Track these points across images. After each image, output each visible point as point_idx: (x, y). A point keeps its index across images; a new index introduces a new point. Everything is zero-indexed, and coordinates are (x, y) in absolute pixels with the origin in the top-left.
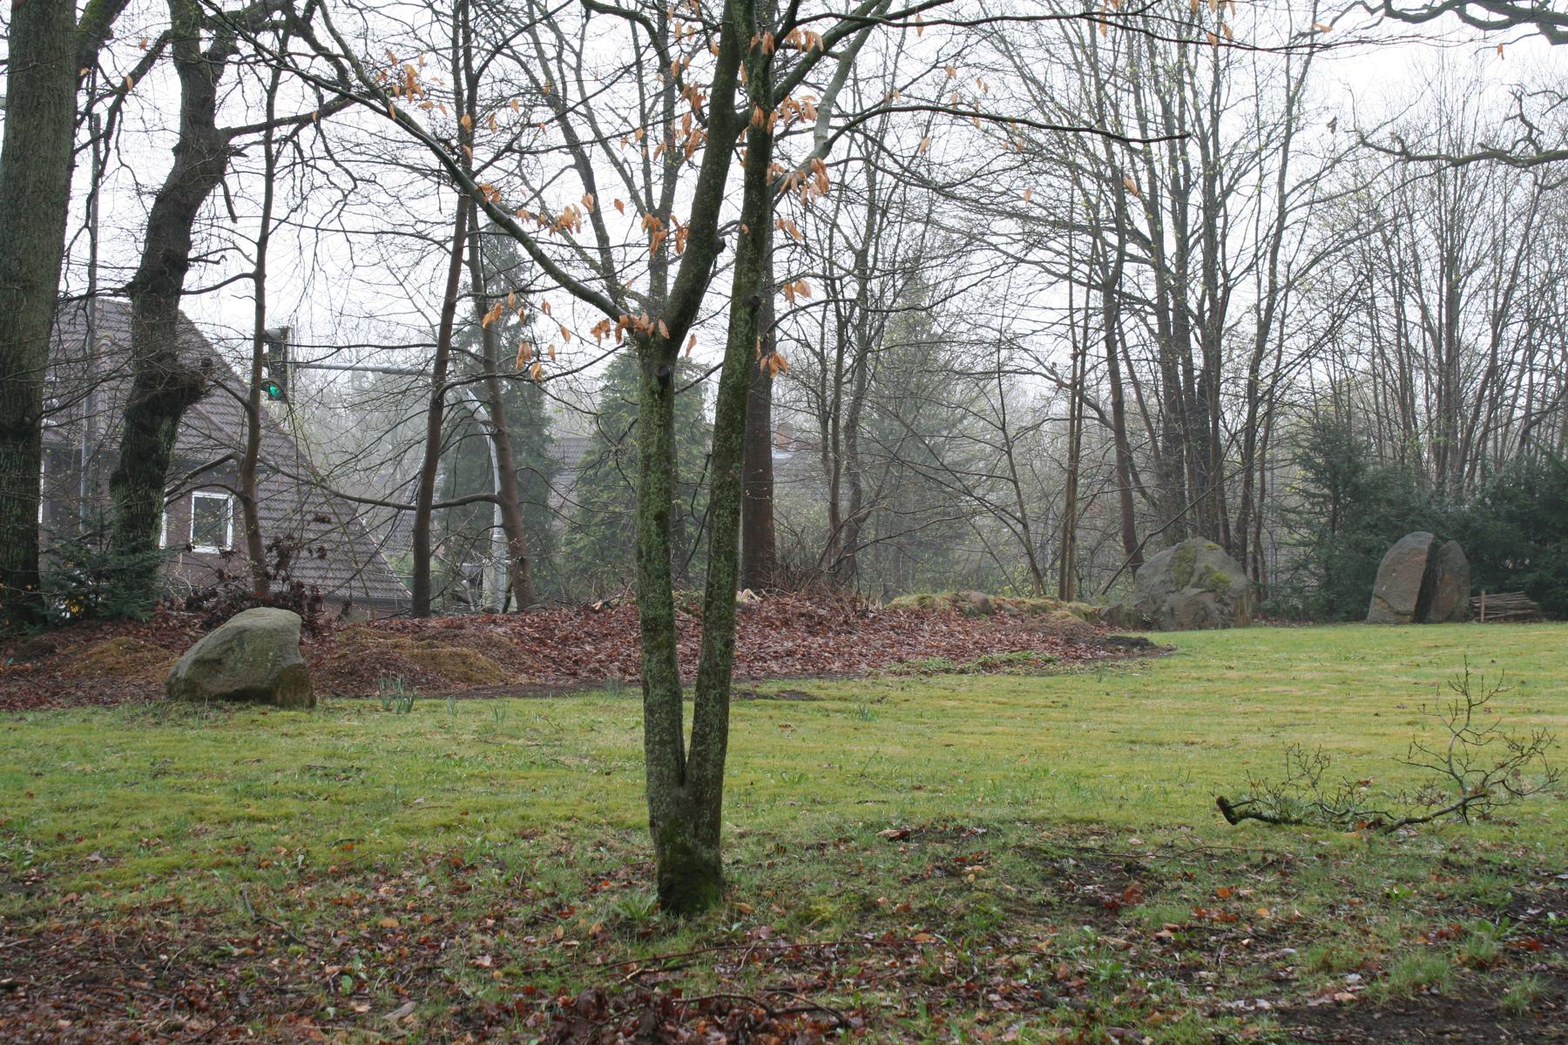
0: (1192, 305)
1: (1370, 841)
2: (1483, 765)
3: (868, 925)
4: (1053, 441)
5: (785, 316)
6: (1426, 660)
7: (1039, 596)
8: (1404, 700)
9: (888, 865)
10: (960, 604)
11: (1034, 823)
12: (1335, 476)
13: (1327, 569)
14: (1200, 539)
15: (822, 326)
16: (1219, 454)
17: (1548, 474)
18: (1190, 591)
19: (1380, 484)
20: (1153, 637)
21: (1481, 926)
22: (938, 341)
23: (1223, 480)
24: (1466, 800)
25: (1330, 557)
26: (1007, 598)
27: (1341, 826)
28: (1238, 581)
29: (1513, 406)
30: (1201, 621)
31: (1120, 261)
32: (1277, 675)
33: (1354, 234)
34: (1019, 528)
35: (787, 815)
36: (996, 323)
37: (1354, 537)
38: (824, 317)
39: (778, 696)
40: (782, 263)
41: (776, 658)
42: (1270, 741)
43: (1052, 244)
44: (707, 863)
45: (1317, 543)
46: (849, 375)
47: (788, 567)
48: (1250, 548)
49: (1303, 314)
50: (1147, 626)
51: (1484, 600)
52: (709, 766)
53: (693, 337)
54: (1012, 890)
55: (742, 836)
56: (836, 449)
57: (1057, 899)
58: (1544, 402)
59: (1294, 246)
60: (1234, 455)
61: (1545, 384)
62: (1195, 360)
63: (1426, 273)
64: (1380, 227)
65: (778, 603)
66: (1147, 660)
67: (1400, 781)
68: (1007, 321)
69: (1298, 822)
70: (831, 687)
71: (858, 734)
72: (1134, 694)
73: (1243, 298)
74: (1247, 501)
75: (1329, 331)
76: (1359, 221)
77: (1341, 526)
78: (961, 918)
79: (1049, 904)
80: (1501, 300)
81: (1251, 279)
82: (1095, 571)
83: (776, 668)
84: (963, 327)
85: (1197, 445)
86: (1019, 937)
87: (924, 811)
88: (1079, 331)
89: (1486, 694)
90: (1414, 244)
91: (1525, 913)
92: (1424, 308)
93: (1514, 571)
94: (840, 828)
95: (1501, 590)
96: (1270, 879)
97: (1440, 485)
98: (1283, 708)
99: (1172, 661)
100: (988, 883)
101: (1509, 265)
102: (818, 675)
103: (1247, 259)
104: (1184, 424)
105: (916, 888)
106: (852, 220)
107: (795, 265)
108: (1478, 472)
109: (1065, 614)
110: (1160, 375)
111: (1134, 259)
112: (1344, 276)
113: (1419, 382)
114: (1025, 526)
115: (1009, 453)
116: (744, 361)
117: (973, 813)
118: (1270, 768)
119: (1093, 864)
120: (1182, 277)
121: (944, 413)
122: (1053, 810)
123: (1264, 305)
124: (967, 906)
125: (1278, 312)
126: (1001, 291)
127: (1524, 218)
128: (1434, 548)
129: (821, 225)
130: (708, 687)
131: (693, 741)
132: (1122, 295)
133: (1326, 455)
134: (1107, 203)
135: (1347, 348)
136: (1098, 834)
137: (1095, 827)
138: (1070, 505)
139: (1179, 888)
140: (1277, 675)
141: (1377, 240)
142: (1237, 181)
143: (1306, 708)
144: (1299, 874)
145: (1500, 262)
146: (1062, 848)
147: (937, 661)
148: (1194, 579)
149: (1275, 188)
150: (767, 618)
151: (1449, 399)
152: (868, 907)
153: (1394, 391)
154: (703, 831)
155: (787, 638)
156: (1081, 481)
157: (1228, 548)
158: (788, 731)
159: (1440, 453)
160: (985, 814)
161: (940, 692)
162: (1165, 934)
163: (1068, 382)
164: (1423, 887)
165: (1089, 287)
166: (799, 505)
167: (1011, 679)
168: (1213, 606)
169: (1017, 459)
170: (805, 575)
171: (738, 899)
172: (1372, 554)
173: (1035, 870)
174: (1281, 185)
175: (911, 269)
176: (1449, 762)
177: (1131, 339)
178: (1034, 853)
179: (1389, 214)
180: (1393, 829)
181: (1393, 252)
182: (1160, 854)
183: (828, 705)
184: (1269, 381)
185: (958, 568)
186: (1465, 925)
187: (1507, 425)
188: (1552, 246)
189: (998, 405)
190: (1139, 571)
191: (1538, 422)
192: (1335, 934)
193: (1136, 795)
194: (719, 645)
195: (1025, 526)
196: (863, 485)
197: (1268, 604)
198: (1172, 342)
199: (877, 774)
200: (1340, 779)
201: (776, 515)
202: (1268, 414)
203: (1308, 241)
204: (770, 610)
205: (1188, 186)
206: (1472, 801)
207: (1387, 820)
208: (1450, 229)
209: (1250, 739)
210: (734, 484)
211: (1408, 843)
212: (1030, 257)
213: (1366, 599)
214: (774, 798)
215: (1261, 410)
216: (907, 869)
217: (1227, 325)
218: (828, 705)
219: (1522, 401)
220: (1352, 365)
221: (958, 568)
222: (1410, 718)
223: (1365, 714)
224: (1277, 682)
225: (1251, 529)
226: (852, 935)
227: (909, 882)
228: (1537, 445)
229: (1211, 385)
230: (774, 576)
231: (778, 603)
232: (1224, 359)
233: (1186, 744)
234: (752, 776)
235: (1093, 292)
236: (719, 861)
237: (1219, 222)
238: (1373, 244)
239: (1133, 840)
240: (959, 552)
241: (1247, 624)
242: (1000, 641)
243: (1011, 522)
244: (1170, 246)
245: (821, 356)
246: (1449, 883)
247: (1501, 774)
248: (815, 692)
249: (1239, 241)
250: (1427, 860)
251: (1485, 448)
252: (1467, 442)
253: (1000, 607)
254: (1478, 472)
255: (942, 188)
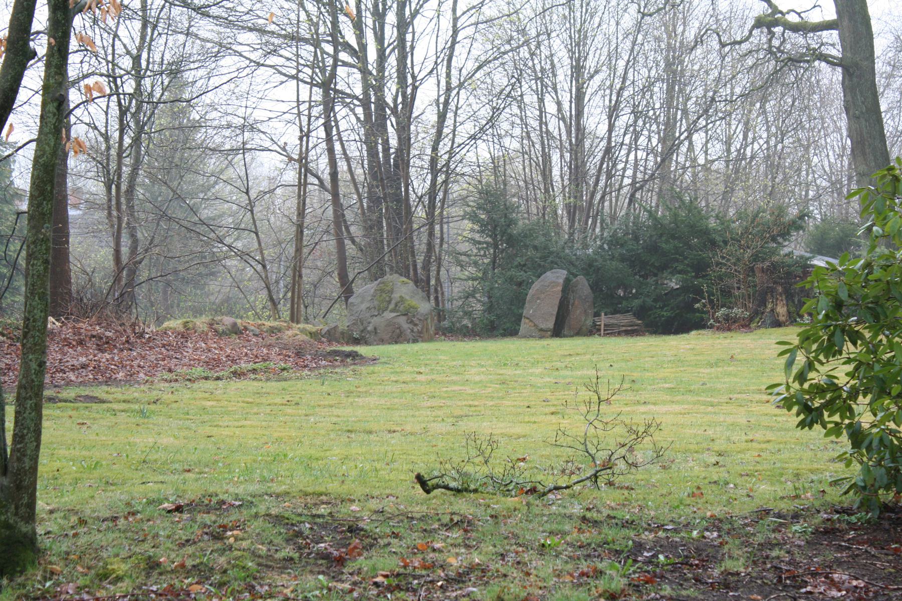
0: (389, 100)
1: (528, 504)
2: (607, 444)
3: (153, 580)
4: (285, 202)
5: (78, 106)
6: (563, 365)
7: (275, 319)
8: (548, 395)
9: (167, 532)
10: (215, 326)
11: (278, 496)
12: (495, 228)
13: (489, 297)
14: (396, 276)
15: (107, 113)
16: (409, 213)
17: (648, 227)
18: (389, 315)
19: (528, 234)
20: (362, 350)
21: (612, 567)
22: (196, 126)
23: (412, 231)
24: (597, 472)
25: (491, 289)
26: (249, 321)
27: (507, 493)
28: (424, 307)
29: (623, 176)
30: (397, 337)
31: (335, 66)
32: (454, 378)
33: (508, 47)
34: (259, 268)
35: (87, 494)
36: (241, 112)
37: (509, 273)
38: (108, 106)
39: (75, 400)
40: (75, 64)
41: (73, 370)
42: (452, 429)
43: (282, 52)
44: (25, 535)
45: (482, 278)
46: (128, 152)
47: (81, 299)
48: (433, 282)
49: (471, 107)
50: (357, 341)
51: (603, 320)
52: (26, 460)
53: (11, 125)
54: (263, 549)
55: (51, 512)
56: (118, 208)
57: (297, 555)
58: (645, 173)
59: (464, 56)
60: (420, 213)
61: (646, 160)
62: (391, 141)
63: (560, 77)
64: (527, 43)
65: (74, 327)
66: (357, 367)
67: (548, 457)
68: (249, 111)
69: (475, 491)
70: (117, 392)
71: (139, 429)
72: (349, 394)
73: (426, 97)
74: (430, 246)
75: (490, 120)
76: (512, 38)
77: (499, 265)
78: (225, 572)
79: (292, 559)
80: (614, 98)
81: (432, 80)
82: (316, 300)
83: (73, 378)
84: (214, 115)
85: (393, 205)
86: (270, 585)
87: (193, 490)
88: (304, 120)
89: (611, 392)
90: (552, 55)
91: (642, 555)
92: (559, 104)
93: (625, 298)
94: (128, 504)
95: (615, 312)
96: (456, 534)
97: (571, 234)
98: (459, 403)
99: (377, 368)
100: (245, 544)
101: (620, 71)
102: (106, 383)
103: (430, 65)
104: (383, 189)
105: (190, 550)
106: (129, 32)
107: (86, 66)
108: (598, 225)
109: (295, 333)
110: (365, 153)
111: (345, 64)
112: (501, 79)
113: (555, 157)
114: (264, 267)
115: (252, 211)
116: (52, 144)
117: (231, 490)
118: (452, 449)
119: (323, 527)
120: (381, 79)
121: (201, 180)
122: (292, 486)
123: (442, 100)
124: (229, 563)
125: (452, 106)
126: (244, 87)
127: (631, 37)
128: (567, 281)
129: (105, 35)
130: (25, 399)
131: (14, 440)
132: (336, 91)
133: (488, 212)
134: (325, 22)
135: (503, 133)
136: (326, 503)
137: (324, 498)
138: (298, 250)
139: (389, 544)
140: (454, 378)
141: (524, 52)
142: (421, 6)
143: (476, 403)
144: (478, 530)
145: (613, 69)
146: (300, 515)
147: (199, 371)
148: (392, 306)
149: (450, 12)
150: (65, 339)
151: (577, 172)
152: (152, 565)
153: (537, 164)
154: (22, 510)
155: (81, 355)
156: (306, 232)
157: (416, 282)
158: (85, 428)
159: (571, 211)
160: (240, 490)
161: (201, 395)
162: (379, 579)
163: (296, 157)
164: (568, 538)
165: (312, 85)
166: (90, 252)
167: (255, 383)
168: (406, 326)
169: (258, 216)
170: (95, 306)
171: (51, 563)
172: (523, 285)
173: (280, 534)
174: (454, 10)
175: (175, 71)
176: (585, 444)
177: (343, 125)
178: (278, 519)
179: (533, 33)
180: (544, 494)
181: (536, 61)
182: (374, 518)
183: (115, 406)
184: (446, 157)
185: (212, 298)
186: (600, 566)
187: (619, 190)
188: (651, 58)
189: (243, 174)
190: (350, 300)
191: (641, 187)
192: (505, 576)
193: (354, 473)
194: (34, 366)
195: (264, 267)
196: (139, 235)
197: (446, 323)
198: (374, 127)
199: (156, 461)
200: (505, 457)
201: (71, 259)
202: (445, 182)
203: (475, 53)
204: (68, 332)
205: (385, 9)
206: (601, 472)
207: (540, 487)
208: (578, 45)
209: (438, 427)
210: (45, 240)
211: (556, 504)
212: (268, 62)
213: (519, 318)
214: (76, 481)
215: (441, 179)
216: (183, 535)
217: (414, 115)
218: (115, 406)
219: (629, 172)
220: (507, 145)
221: (212, 298)
222: (553, 409)
223: (520, 407)
224: (454, 383)
225: (434, 268)
226: (140, 588)
227: (184, 545)
228: (641, 205)
229: (403, 160)
230: (71, 306)
231: (74, 327)
232: (412, 141)
233: (390, 431)
234: (57, 464)
235: (315, 89)
236: (35, 533)
237: (409, 37)
238: (521, 55)
239: (353, 508)
240: (213, 286)
241: (430, 339)
242: (246, 354)
243: (253, 263)
244: (372, 55)
245: (107, 138)
246: (587, 535)
247: (623, 451)
248: (104, 396)
249: (424, 51)
250: (570, 517)
251: (603, 207)
252: (590, 204)
253: (246, 329)
254: (598, 225)
255: (199, 8)
